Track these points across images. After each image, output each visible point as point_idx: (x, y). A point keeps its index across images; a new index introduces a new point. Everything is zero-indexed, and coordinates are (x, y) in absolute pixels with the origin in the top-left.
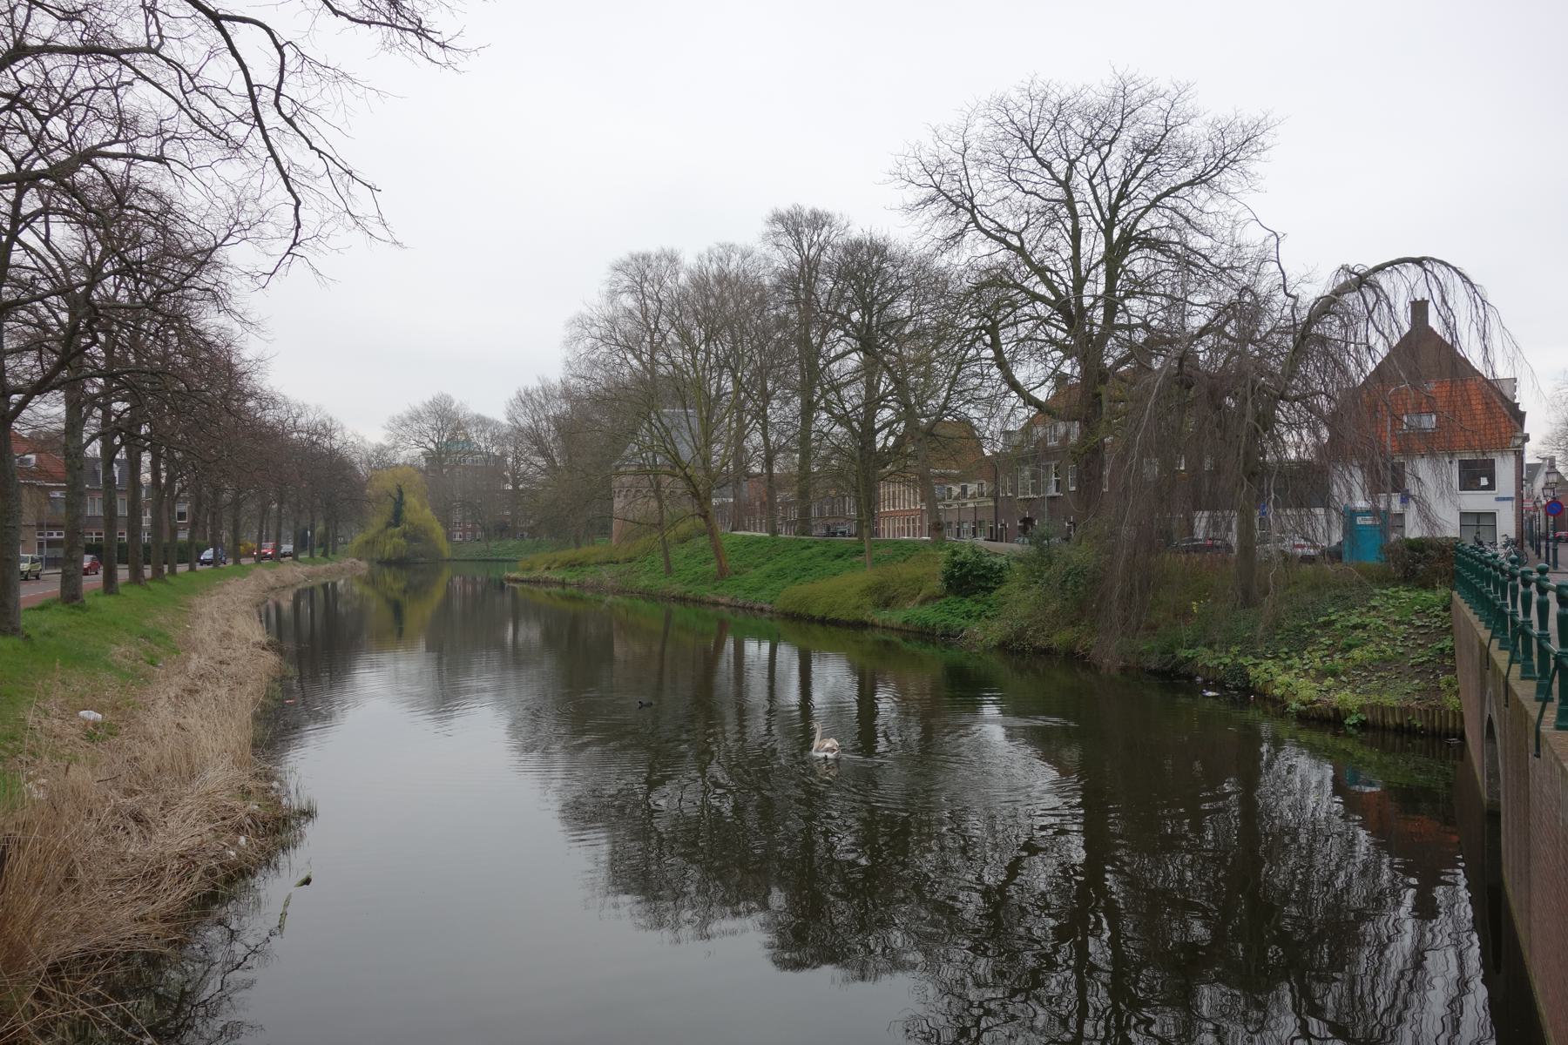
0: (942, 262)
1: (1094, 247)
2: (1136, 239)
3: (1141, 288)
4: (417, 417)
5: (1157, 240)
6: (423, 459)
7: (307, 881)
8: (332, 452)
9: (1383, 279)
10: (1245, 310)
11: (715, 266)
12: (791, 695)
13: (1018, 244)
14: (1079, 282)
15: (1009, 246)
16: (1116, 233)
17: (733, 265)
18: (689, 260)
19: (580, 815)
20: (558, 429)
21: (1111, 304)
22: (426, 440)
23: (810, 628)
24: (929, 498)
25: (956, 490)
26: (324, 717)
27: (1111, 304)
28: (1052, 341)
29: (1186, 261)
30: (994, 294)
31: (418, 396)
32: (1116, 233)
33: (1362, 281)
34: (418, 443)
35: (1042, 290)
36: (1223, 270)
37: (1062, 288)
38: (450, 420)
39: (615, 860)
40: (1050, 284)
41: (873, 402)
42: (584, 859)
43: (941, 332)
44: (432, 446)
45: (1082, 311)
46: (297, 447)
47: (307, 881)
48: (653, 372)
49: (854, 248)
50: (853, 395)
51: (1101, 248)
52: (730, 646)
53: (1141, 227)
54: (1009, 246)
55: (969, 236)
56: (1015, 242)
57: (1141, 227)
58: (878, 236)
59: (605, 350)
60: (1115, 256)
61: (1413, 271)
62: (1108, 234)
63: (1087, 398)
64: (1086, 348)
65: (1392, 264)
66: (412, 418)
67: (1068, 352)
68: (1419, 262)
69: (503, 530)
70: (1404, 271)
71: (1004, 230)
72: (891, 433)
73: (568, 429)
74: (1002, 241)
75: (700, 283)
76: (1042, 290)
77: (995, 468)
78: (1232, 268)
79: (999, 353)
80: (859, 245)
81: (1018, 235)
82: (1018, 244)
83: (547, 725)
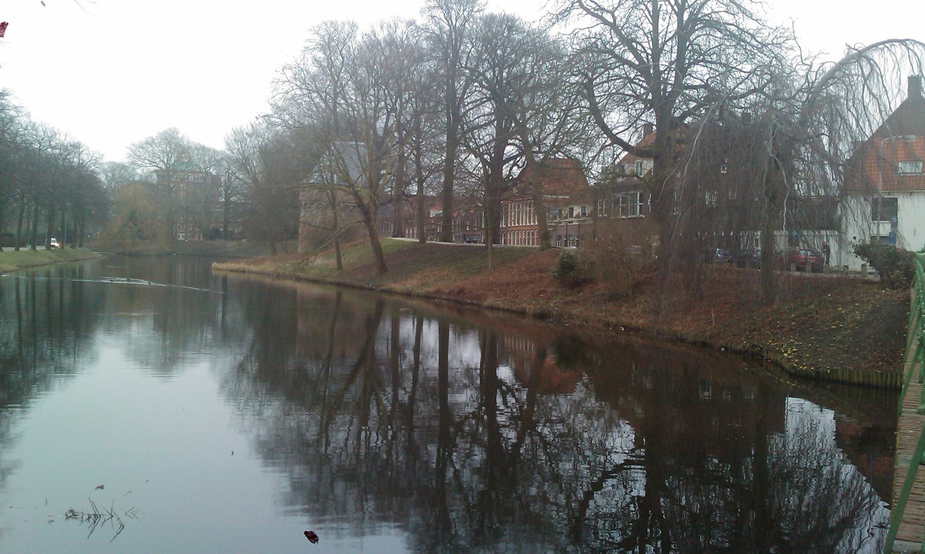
0: (553, 33)
1: (669, 25)
2: (700, 20)
3: (702, 57)
4: (150, 143)
5: (718, 22)
6: (155, 176)
7: (102, 487)
8: (81, 166)
9: (876, 56)
10: (777, 78)
11: (386, 32)
12: (432, 363)
13: (611, 20)
14: (657, 52)
15: (605, 22)
16: (686, 16)
17: (399, 32)
18: (364, 29)
19: (271, 451)
20: (261, 152)
21: (681, 68)
22: (157, 160)
23: (457, 313)
24: (541, 215)
25: (565, 212)
26: (69, 372)
27: (681, 68)
28: (638, 97)
29: (739, 39)
30: (593, 57)
31: (153, 129)
32: (686, 16)
33: (860, 56)
34: (151, 162)
35: (630, 56)
36: (766, 45)
37: (644, 55)
38: (178, 145)
39: (296, 486)
40: (634, 51)
41: (501, 142)
42: (263, 487)
43: (553, 85)
44: (162, 165)
45: (659, 73)
46: (51, 162)
47: (102, 487)
48: (334, 111)
49: (490, 21)
50: (487, 134)
51: (674, 27)
52: (386, 327)
53: (706, 11)
54: (605, 22)
55: (575, 12)
56: (609, 17)
57: (706, 11)
58: (509, 12)
59: (298, 92)
60: (683, 34)
61: (899, 50)
62: (680, 15)
63: (662, 144)
64: (661, 103)
65: (883, 43)
66: (147, 143)
67: (649, 105)
68: (902, 42)
69: (214, 235)
70: (893, 49)
71: (603, 9)
72: (515, 164)
73: (265, 152)
74: (601, 18)
75: (373, 45)
76: (630, 56)
77: (599, 193)
78: (773, 44)
79: (594, 105)
80: (492, 18)
81: (612, 13)
82: (611, 20)
83: (245, 384)
